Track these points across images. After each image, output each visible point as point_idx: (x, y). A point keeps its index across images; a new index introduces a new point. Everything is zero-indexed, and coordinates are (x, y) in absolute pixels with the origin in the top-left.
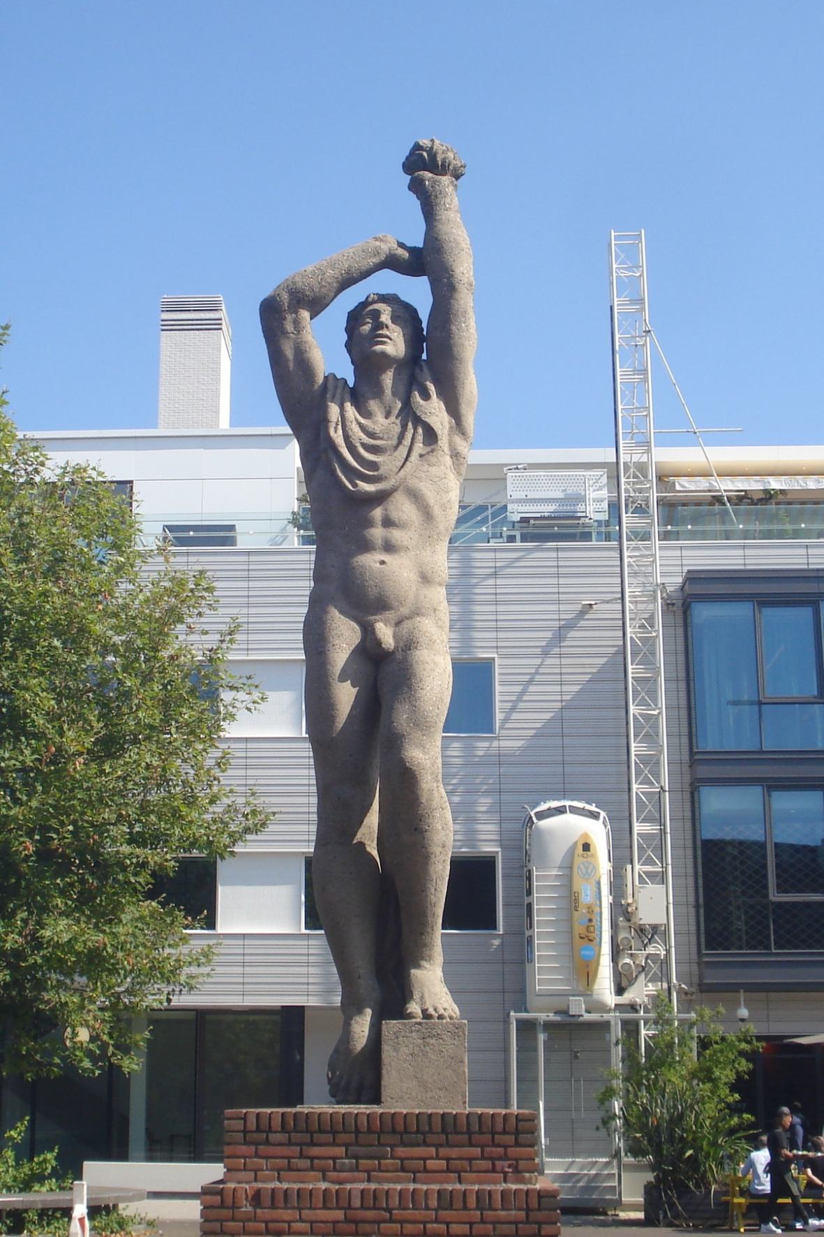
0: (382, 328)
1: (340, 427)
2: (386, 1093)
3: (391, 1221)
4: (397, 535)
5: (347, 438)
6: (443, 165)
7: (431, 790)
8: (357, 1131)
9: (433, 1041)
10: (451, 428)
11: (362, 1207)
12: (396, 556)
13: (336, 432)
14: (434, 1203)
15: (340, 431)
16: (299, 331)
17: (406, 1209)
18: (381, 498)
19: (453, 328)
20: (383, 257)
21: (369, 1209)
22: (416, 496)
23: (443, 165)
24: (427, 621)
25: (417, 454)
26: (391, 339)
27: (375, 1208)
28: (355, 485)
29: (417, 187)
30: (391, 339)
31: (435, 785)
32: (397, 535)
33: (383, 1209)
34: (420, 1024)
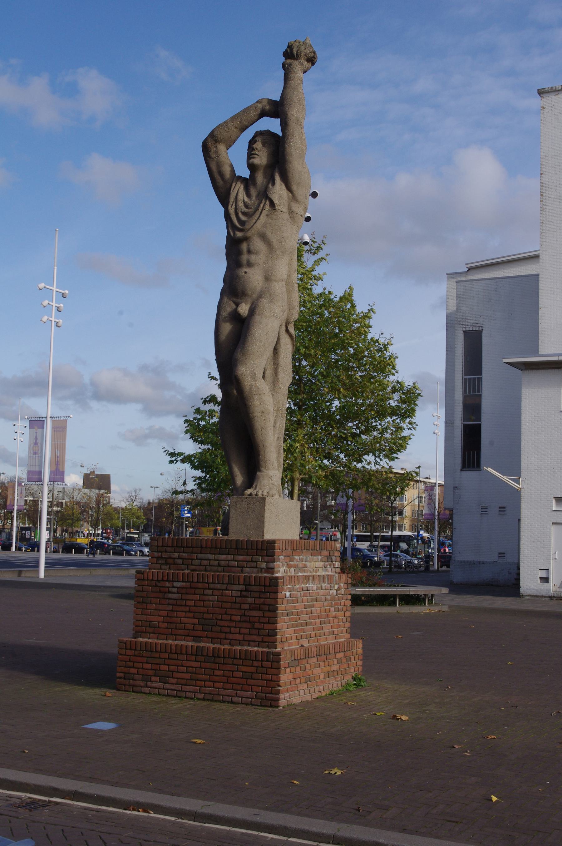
0: (254, 150)
1: (234, 204)
2: (231, 531)
3: (209, 589)
4: (253, 258)
5: (236, 209)
6: (297, 55)
7: (251, 386)
8: (202, 547)
9: (251, 506)
10: (289, 198)
11: (198, 582)
12: (253, 269)
13: (231, 207)
14: (226, 581)
15: (234, 207)
16: (218, 157)
17: (215, 583)
18: (246, 239)
19: (286, 145)
20: (259, 111)
21: (200, 582)
22: (263, 237)
23: (297, 55)
24: (265, 301)
25: (265, 215)
26: (258, 155)
27: (202, 582)
28: (234, 234)
29: (287, 70)
30: (258, 155)
31: (254, 383)
32: (253, 258)
33: (206, 583)
34: (246, 498)
